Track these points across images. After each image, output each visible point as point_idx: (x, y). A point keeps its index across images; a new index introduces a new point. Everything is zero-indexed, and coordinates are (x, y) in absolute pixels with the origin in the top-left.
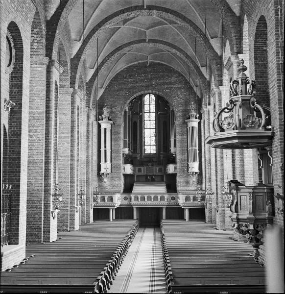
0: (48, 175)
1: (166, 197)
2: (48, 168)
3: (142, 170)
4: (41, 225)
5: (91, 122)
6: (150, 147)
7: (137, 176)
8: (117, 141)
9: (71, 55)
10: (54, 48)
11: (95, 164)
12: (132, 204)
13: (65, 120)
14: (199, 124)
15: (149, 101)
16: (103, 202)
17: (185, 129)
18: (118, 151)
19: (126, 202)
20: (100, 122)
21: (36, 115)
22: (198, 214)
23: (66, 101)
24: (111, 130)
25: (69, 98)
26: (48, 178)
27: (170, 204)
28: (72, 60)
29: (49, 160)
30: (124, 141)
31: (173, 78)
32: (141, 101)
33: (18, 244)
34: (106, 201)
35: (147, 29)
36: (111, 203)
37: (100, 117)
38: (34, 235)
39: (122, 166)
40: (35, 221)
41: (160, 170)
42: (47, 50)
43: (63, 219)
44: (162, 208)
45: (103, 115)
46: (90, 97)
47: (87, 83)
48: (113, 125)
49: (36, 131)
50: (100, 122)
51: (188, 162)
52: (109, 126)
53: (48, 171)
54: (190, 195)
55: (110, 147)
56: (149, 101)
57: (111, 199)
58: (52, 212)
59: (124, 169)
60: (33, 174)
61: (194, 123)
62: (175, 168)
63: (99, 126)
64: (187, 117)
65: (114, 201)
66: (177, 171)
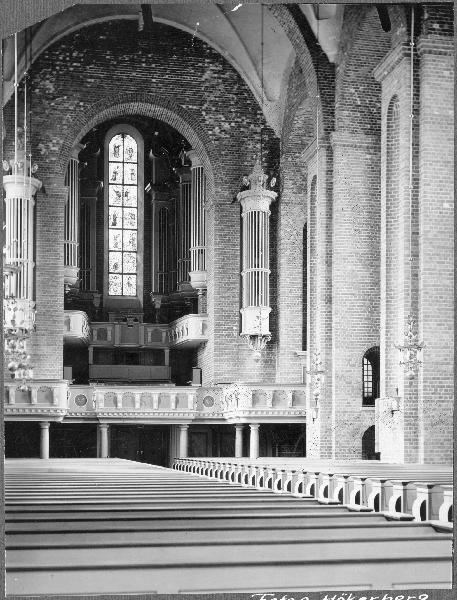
3: (109, 333)
6: (125, 279)
7: (96, 350)
8: (50, 242)
12: (100, 415)
14: (275, 206)
15: (124, 154)
16: (24, 405)
17: (236, 217)
18: (53, 273)
19: (82, 411)
22: (285, 439)
27: (202, 416)
30: (67, 247)
31: (207, 75)
32: (102, 150)
33: (303, 454)
34: (35, 400)
39: (63, 314)
41: (156, 336)
44: (178, 427)
51: (241, 307)
54: (286, 389)
56: (124, 154)
57: (50, 397)
59: (68, 323)
61: (258, 202)
62: (204, 327)
64: (238, 183)
65: (56, 400)
66: (210, 336)
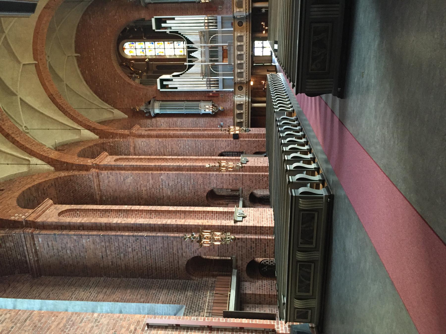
0: (184, 228)
1: (239, 34)
2: (175, 228)
4: (251, 239)
5: (146, 133)
9: (49, 172)
10: (13, 218)
11: (202, 121)
13: (131, 178)
20: (152, 114)
21: (103, 244)
23: (108, 177)
24: (163, 101)
25: (104, 173)
26: (189, 228)
28: (57, 169)
29: (164, 227)
35: (19, 62)
36: (244, 106)
37: (147, 115)
38: (265, 247)
40: (246, 246)
42: (17, 228)
43: (254, 181)
45: (145, 111)
46: (117, 134)
47: (100, 138)
48: (156, 100)
49: (125, 244)
50: (152, 114)
52: (157, 104)
53: (180, 228)
55: (183, 103)
57: (240, 106)
58: (236, 222)
60: (184, 248)
63: (157, 115)
